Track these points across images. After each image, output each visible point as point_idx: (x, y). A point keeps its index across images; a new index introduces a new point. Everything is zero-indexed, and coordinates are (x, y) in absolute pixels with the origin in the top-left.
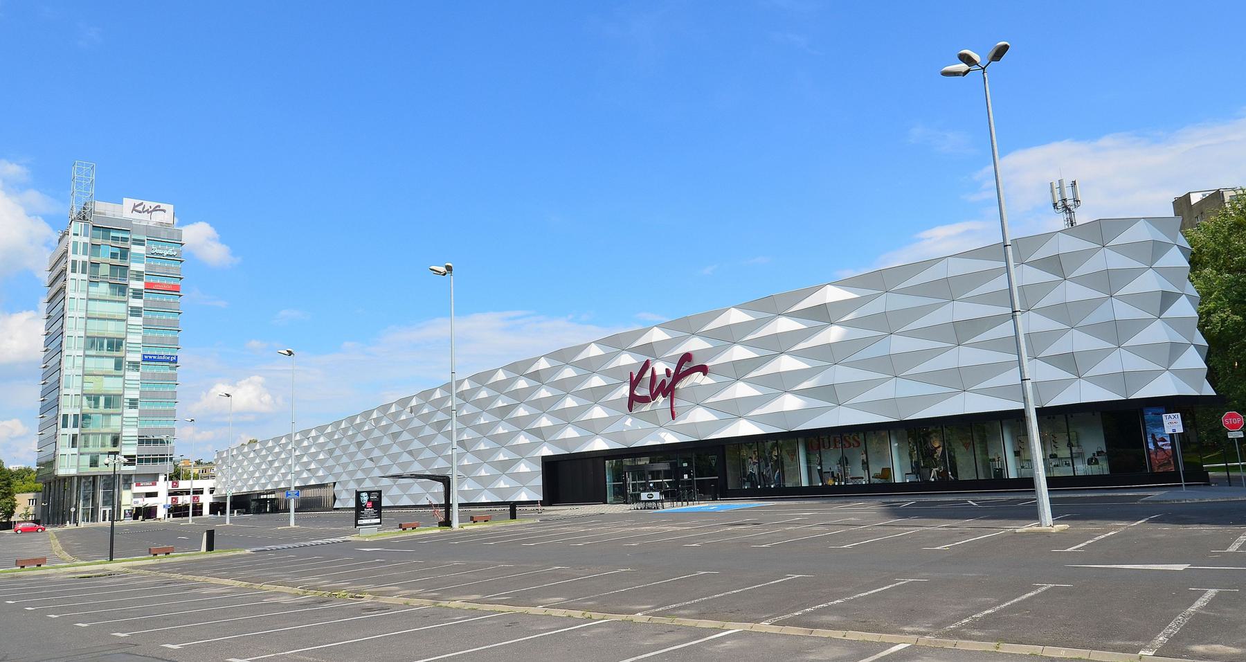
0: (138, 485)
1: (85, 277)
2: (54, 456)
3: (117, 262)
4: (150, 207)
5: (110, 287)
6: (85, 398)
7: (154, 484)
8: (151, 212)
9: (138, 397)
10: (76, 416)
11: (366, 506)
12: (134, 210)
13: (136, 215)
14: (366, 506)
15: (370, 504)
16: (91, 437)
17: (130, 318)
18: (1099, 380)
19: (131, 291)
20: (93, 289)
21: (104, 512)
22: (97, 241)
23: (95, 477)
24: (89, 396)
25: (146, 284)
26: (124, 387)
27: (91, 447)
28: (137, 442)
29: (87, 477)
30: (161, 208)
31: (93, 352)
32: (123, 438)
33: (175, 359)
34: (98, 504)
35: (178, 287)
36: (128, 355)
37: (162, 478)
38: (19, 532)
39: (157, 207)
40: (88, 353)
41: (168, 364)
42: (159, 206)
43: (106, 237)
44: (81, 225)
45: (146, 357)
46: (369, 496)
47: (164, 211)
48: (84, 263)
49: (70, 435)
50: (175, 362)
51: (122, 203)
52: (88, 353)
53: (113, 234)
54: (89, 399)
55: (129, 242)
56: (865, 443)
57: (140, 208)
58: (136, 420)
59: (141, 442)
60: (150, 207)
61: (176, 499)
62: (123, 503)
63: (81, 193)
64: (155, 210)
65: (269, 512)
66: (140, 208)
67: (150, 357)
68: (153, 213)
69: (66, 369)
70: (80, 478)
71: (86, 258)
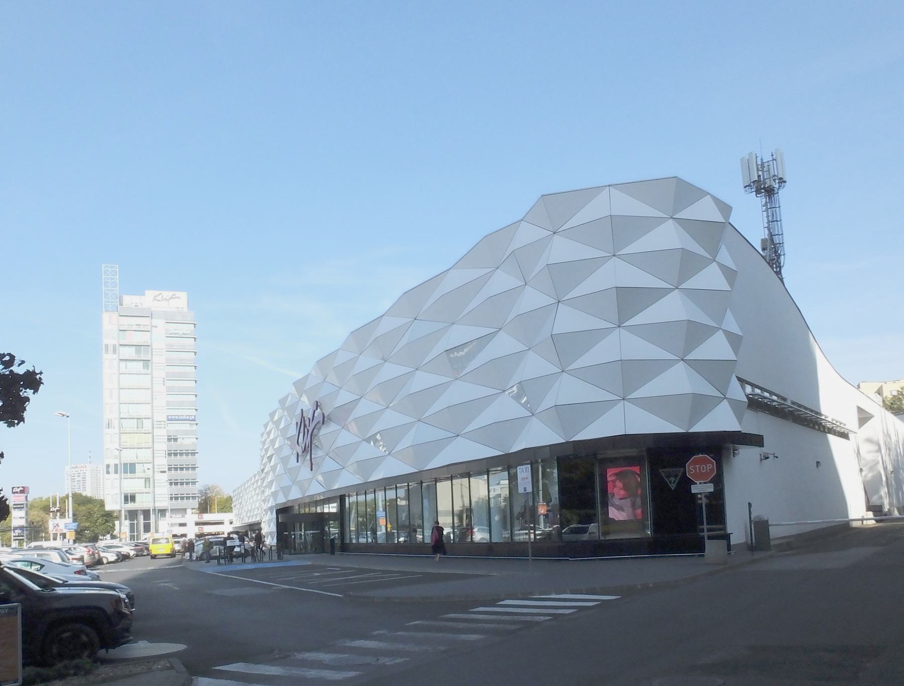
4: (168, 296)
10: (116, 465)
18: (650, 404)
28: (166, 440)
30: (176, 296)
37: (189, 511)
39: (173, 295)
41: (189, 422)
42: (175, 295)
45: (170, 417)
47: (178, 298)
51: (144, 295)
56: (816, 342)
57: (159, 298)
59: (169, 440)
60: (168, 296)
61: (202, 528)
63: (113, 279)
64: (171, 298)
65: (376, 434)
68: (171, 300)
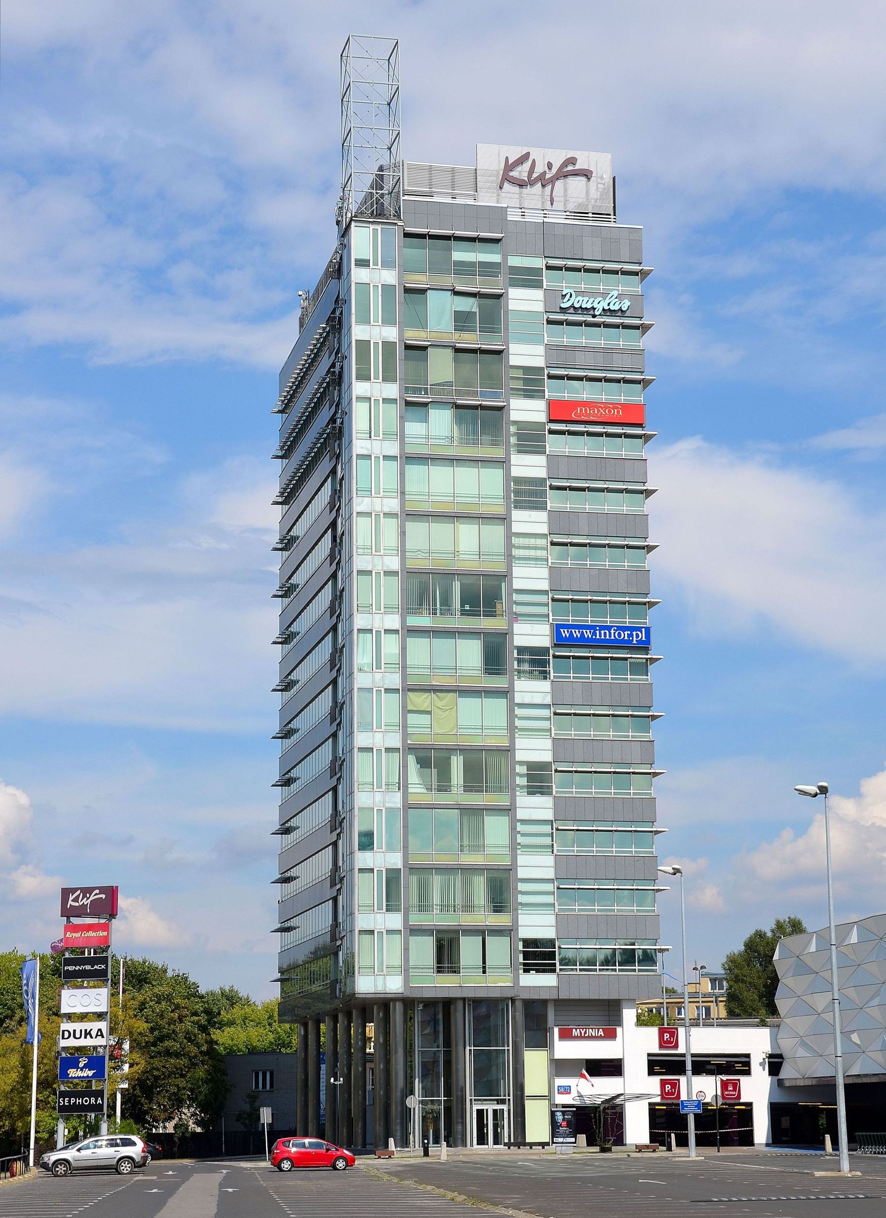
0: (566, 1035)
1: (392, 390)
2: (334, 938)
3: (470, 340)
4: (550, 166)
5: (459, 421)
6: (411, 759)
7: (610, 1035)
8: (553, 180)
9: (547, 757)
11: (561, 1124)
12: (506, 178)
13: (510, 197)
14: (561, 1124)
15: (564, 1123)
16: (437, 881)
17: (516, 515)
19: (513, 429)
20: (414, 428)
21: (480, 1113)
22: (418, 280)
23: (447, 1004)
24: (422, 754)
25: (552, 405)
26: (512, 729)
27: (436, 911)
29: (430, 1004)
30: (578, 167)
31: (423, 621)
32: (521, 887)
33: (642, 636)
34: (463, 1090)
35: (639, 408)
36: (518, 628)
37: (629, 1015)
38: (286, 1165)
39: (566, 163)
40: (414, 621)
42: (572, 161)
43: (438, 267)
44: (375, 230)
45: (565, 633)
46: (564, 1115)
48: (388, 346)
49: (380, 871)
50: (644, 647)
52: (414, 621)
53: (460, 255)
54: (424, 763)
55: (500, 278)
58: (547, 829)
62: (527, 1092)
66: (521, 173)
67: (576, 633)
68: (559, 184)
69: (360, 670)
70: (408, 1003)
71: (391, 334)
